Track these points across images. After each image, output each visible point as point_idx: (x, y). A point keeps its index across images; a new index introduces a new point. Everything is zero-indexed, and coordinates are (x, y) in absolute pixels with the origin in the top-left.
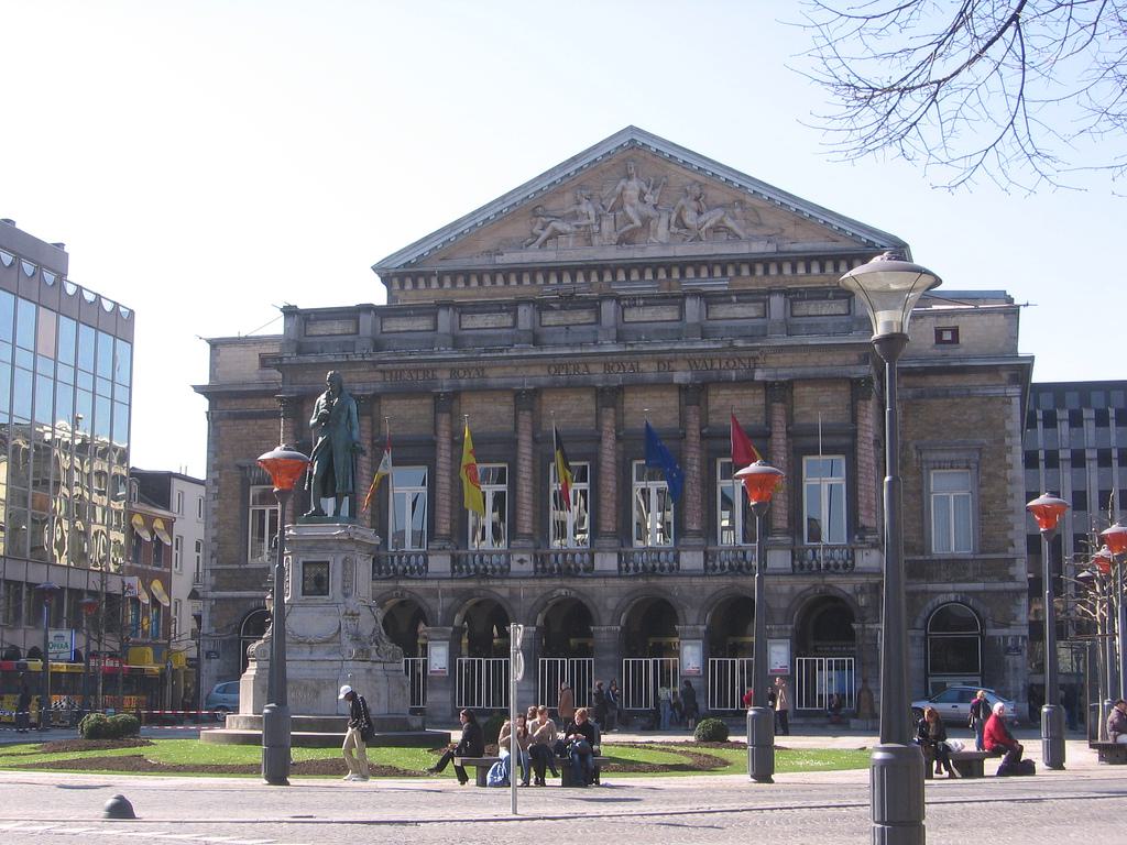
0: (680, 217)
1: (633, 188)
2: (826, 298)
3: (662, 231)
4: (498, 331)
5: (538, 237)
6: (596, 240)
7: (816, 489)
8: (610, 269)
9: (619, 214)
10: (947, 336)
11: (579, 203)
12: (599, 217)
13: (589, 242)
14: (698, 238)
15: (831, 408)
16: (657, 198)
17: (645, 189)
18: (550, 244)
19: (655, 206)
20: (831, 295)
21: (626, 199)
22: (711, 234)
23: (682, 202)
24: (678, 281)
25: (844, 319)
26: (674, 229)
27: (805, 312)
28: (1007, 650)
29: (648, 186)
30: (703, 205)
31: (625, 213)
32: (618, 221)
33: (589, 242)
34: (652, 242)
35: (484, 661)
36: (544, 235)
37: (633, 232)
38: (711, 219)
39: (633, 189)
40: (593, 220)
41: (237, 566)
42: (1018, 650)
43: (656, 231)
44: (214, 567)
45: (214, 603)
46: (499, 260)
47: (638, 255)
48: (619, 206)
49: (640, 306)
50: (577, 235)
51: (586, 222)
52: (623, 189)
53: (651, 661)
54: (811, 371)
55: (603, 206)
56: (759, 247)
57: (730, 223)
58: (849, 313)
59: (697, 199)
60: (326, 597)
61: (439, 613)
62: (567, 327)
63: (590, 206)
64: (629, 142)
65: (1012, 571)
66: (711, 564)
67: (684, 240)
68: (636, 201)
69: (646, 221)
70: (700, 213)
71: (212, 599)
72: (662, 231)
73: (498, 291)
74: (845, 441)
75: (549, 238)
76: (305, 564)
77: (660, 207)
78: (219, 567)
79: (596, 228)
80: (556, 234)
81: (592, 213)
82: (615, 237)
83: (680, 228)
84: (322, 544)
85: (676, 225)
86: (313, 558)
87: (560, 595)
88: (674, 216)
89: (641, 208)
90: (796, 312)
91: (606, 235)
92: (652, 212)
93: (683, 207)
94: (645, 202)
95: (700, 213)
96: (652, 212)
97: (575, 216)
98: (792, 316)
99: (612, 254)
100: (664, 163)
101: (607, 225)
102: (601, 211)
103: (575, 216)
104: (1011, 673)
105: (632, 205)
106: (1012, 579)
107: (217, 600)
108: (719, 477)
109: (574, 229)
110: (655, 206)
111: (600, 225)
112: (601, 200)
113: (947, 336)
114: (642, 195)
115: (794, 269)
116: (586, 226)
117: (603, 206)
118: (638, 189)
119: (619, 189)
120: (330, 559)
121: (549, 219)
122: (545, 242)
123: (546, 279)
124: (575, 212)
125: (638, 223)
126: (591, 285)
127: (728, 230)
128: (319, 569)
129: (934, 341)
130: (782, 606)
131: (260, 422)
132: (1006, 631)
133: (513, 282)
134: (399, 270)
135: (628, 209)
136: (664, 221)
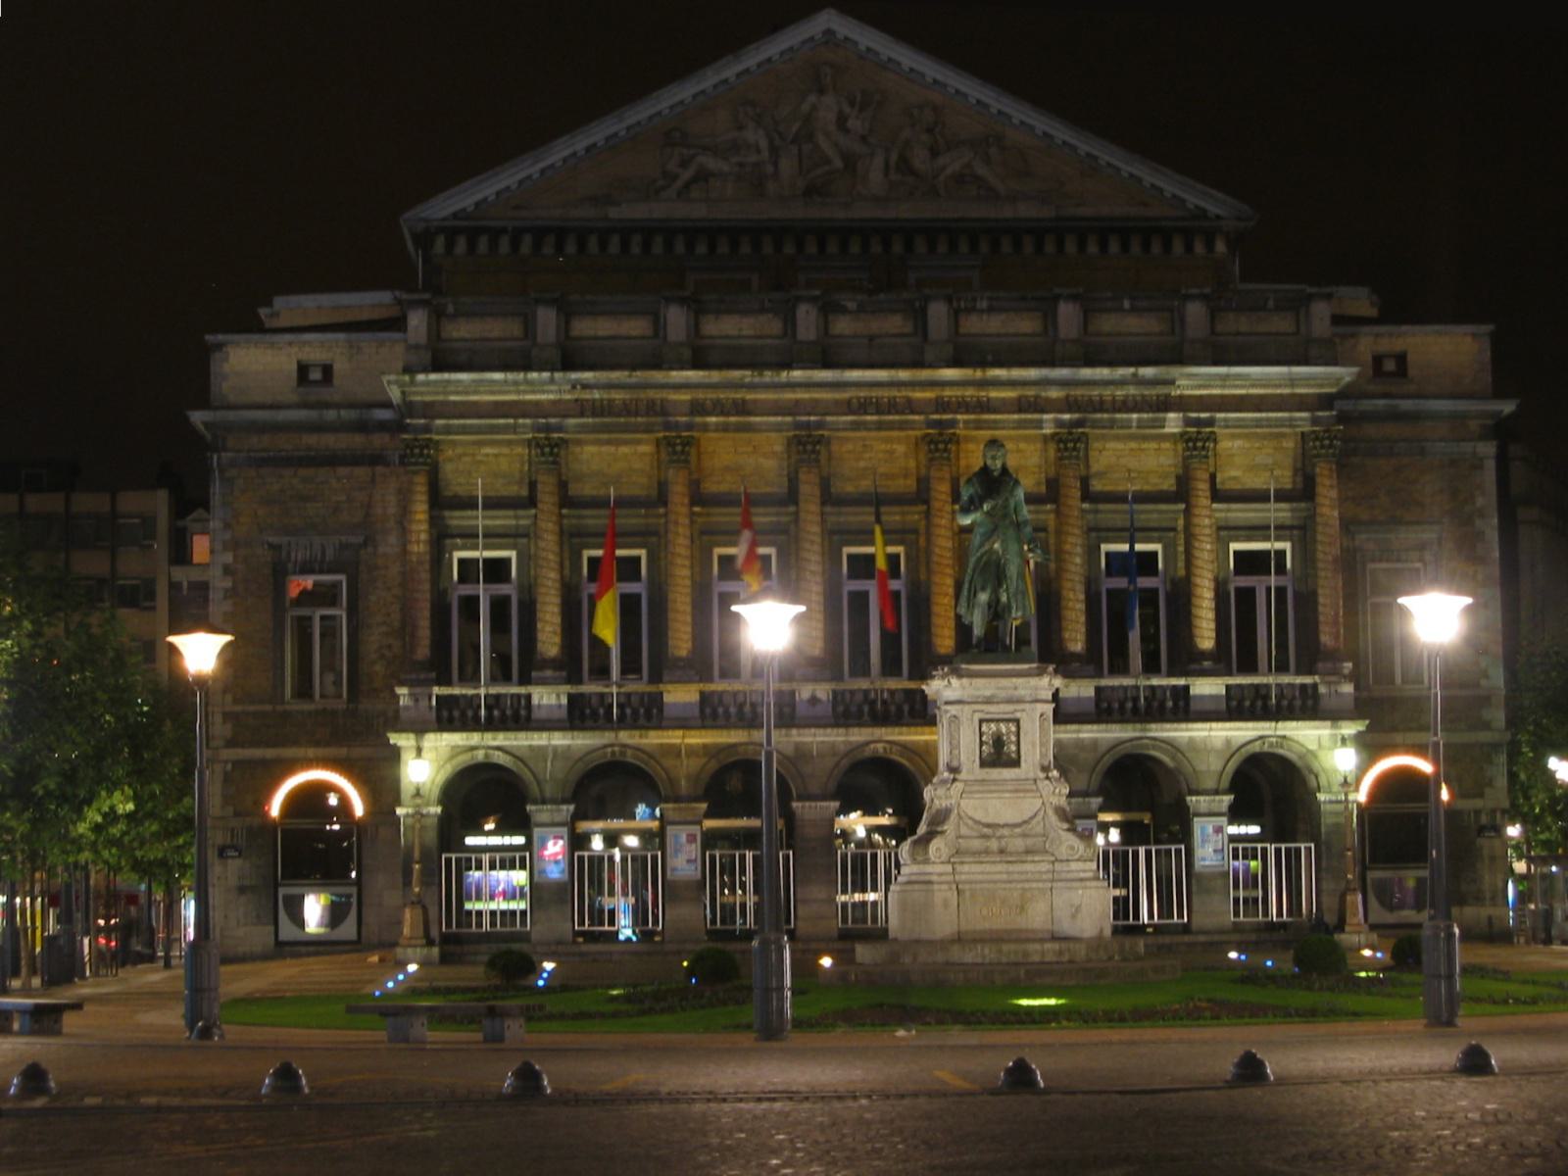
1: (828, 108)
4: (760, 342)
5: (675, 177)
10: (1390, 366)
11: (740, 128)
12: (774, 151)
17: (847, 109)
28: (1481, 830)
35: (1142, 850)
36: (687, 175)
38: (953, 163)
40: (766, 154)
41: (268, 708)
42: (222, 852)
44: (228, 709)
45: (229, 767)
46: (614, 213)
47: (840, 214)
49: (982, 311)
51: (753, 158)
52: (814, 108)
53: (1142, 850)
56: (1026, 211)
57: (981, 170)
59: (930, 131)
60: (1016, 770)
61: (683, 783)
62: (871, 338)
65: (1487, 714)
66: (1105, 705)
69: (850, 161)
70: (934, 153)
71: (226, 762)
72: (875, 177)
75: (695, 180)
76: (981, 721)
78: (238, 708)
79: (770, 169)
80: (703, 176)
81: (764, 144)
86: (995, 710)
87: (876, 750)
88: (894, 157)
95: (934, 153)
98: (1213, 332)
99: (798, 211)
101: (787, 165)
104: (1487, 861)
106: (1486, 726)
107: (236, 764)
110: (863, 139)
111: (776, 164)
113: (1390, 366)
114: (841, 121)
115: (1082, 245)
119: (805, 107)
121: (692, 152)
122: (687, 186)
123: (690, 246)
125: (838, 163)
129: (1371, 372)
130: (1213, 768)
131: (303, 472)
132: (1478, 803)
134: (447, 223)
135: (821, 139)
136: (878, 161)
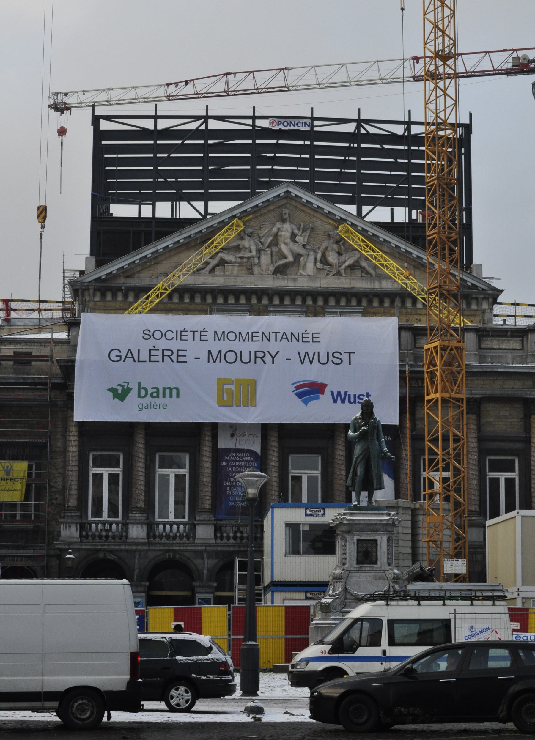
0: (324, 255)
1: (286, 229)
2: (506, 336)
3: (310, 266)
6: (256, 270)
7: (165, 479)
8: (268, 295)
9: (275, 249)
12: (259, 251)
13: (250, 271)
14: (338, 274)
15: (510, 420)
16: (306, 240)
17: (296, 231)
18: (218, 271)
19: (304, 246)
20: (509, 333)
21: (281, 239)
22: (349, 271)
23: (325, 244)
24: (322, 307)
25: (520, 353)
26: (319, 265)
27: (489, 346)
29: (299, 229)
30: (342, 247)
31: (280, 250)
32: (274, 254)
33: (250, 271)
34: (301, 275)
36: (214, 262)
37: (286, 266)
39: (287, 230)
40: (254, 253)
43: (305, 266)
48: (275, 242)
50: (240, 265)
51: (248, 255)
52: (279, 229)
54: (497, 392)
55: (261, 242)
58: (522, 349)
59: (337, 242)
63: (252, 242)
64: (285, 192)
67: (328, 274)
68: (288, 240)
70: (340, 254)
72: (310, 266)
73: (173, 306)
74: (519, 446)
75: (217, 265)
77: (308, 247)
79: (256, 260)
81: (253, 248)
82: (272, 268)
83: (324, 264)
84: (372, 527)
85: (321, 262)
88: (319, 256)
89: (292, 246)
90: (483, 346)
91: (264, 268)
92: (302, 251)
93: (326, 248)
94: (296, 242)
96: (302, 251)
97: (238, 249)
100: (312, 213)
101: (265, 259)
102: (260, 247)
103: (238, 249)
105: (286, 244)
108: (157, 466)
109: (239, 260)
110: (304, 246)
111: (259, 258)
112: (260, 238)
114: (293, 236)
116: (249, 258)
117: (261, 242)
118: (290, 231)
119: (275, 230)
120: (378, 537)
124: (239, 245)
125: (291, 259)
126: (252, 305)
127: (363, 269)
128: (365, 545)
133: (187, 300)
136: (312, 258)
